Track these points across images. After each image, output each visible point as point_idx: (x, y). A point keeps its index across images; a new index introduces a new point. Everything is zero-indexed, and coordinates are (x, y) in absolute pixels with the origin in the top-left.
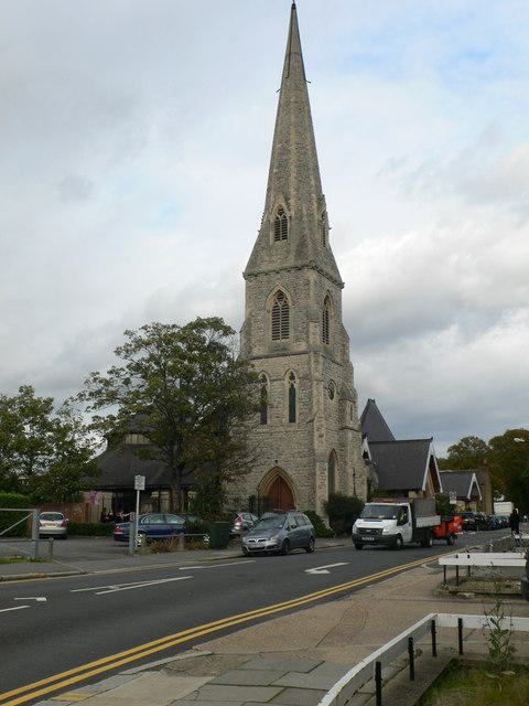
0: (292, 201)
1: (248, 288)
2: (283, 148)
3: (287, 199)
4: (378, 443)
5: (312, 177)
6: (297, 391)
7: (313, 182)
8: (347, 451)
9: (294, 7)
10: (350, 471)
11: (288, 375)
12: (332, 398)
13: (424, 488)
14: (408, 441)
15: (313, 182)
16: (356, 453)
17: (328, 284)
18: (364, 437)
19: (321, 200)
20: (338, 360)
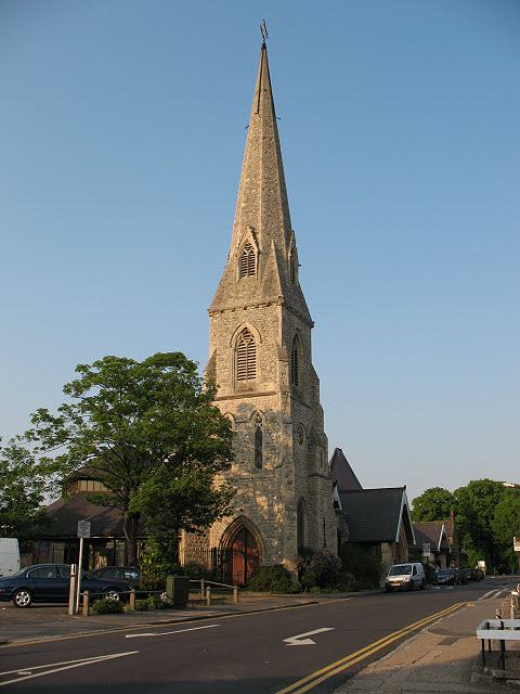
0: (259, 236)
9: (264, 47)
10: (320, 521)
12: (301, 443)
13: (397, 540)
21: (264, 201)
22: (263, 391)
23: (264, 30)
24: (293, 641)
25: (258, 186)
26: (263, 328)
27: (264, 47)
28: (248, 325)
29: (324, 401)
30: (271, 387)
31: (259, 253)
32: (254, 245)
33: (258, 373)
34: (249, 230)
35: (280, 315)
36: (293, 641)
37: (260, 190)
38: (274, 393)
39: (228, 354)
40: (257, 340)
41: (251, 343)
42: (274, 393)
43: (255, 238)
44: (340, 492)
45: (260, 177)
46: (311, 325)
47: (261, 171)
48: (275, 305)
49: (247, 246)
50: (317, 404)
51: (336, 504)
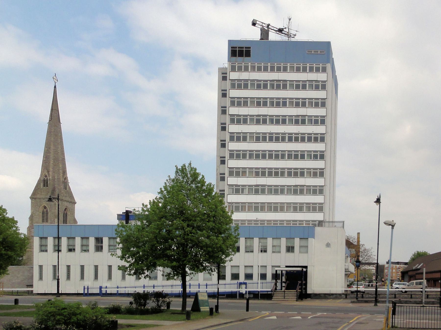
0: (51, 173)
3: (48, 172)
9: (55, 87)
27: (55, 87)
33: (49, 221)
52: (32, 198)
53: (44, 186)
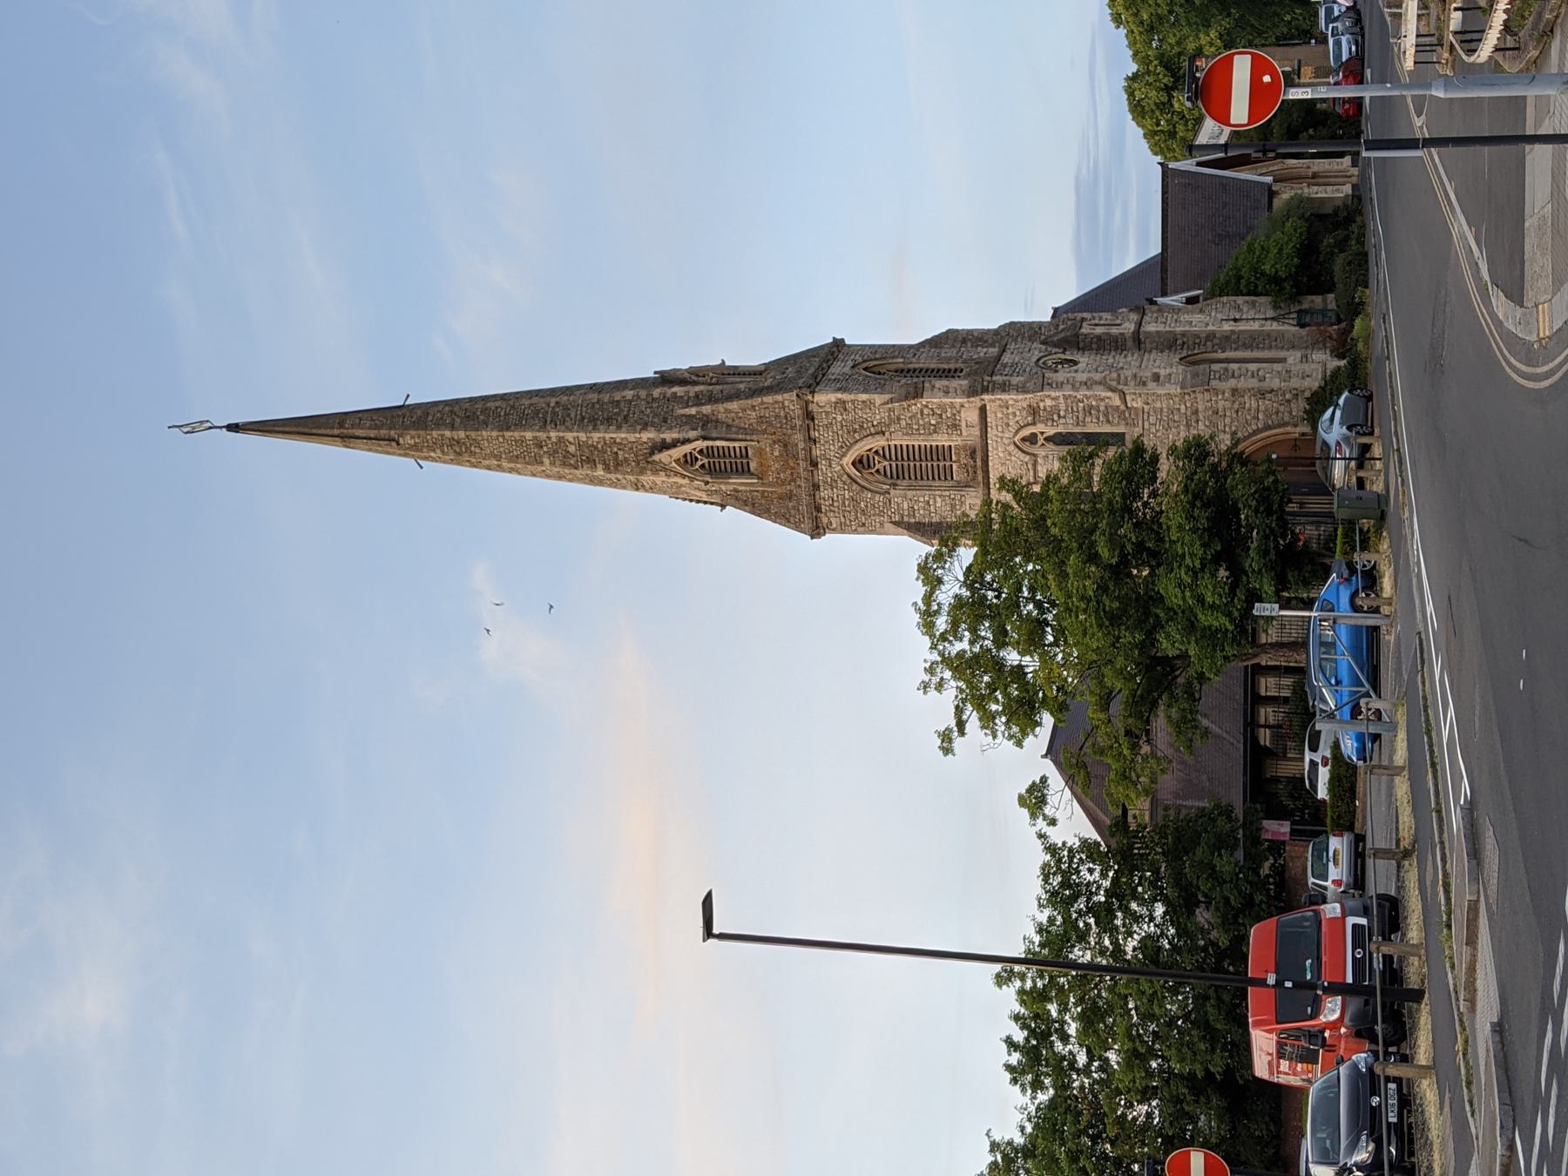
0: (669, 436)
1: (843, 529)
2: (552, 454)
3: (664, 446)
4: (365, 438)
5: (617, 396)
6: (1061, 429)
7: (629, 394)
8: (1184, 334)
9: (234, 428)
10: (1227, 327)
11: (1026, 446)
12: (1075, 363)
13: (1269, 179)
14: (1164, 193)
15: (629, 394)
16: (1139, 770)
17: (837, 369)
18: (1152, 303)
19: (666, 379)
20: (994, 351)
21: (595, 429)
22: (976, 432)
23: (191, 429)
24: (1524, 651)
25: (560, 439)
26: (859, 430)
27: (234, 428)
28: (847, 460)
29: (990, 321)
30: (970, 416)
31: (705, 438)
32: (687, 448)
33: (941, 440)
34: (657, 457)
35: (833, 397)
36: (1524, 651)
37: (570, 436)
38: (983, 410)
39: (903, 499)
40: (878, 443)
41: (881, 453)
42: (983, 410)
43: (675, 444)
44: (1164, 294)
45: (542, 435)
46: (838, 344)
47: (529, 435)
48: (811, 407)
49: (688, 460)
50: (996, 332)
51: (1191, 301)
52: (816, 531)
53: (744, 471)
